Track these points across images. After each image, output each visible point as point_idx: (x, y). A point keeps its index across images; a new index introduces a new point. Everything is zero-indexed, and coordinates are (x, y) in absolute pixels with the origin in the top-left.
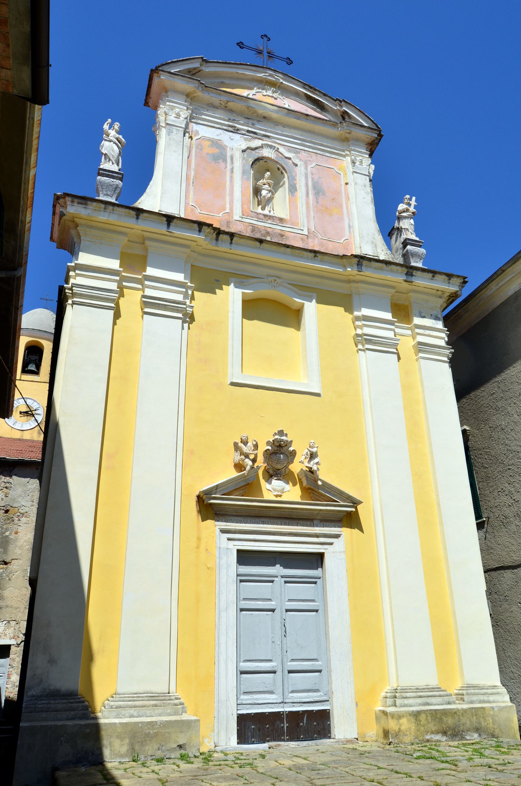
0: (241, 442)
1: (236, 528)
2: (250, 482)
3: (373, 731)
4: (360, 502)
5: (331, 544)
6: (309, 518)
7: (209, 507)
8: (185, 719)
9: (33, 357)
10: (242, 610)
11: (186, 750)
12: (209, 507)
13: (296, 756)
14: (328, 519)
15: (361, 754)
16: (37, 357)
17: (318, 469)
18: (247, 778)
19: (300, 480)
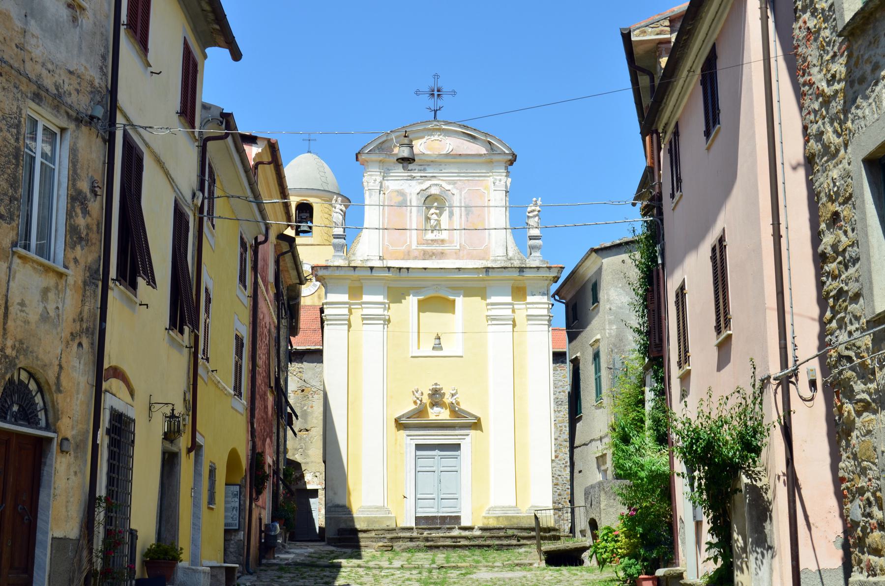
9: (304, 215)
12: (400, 425)
16: (308, 215)
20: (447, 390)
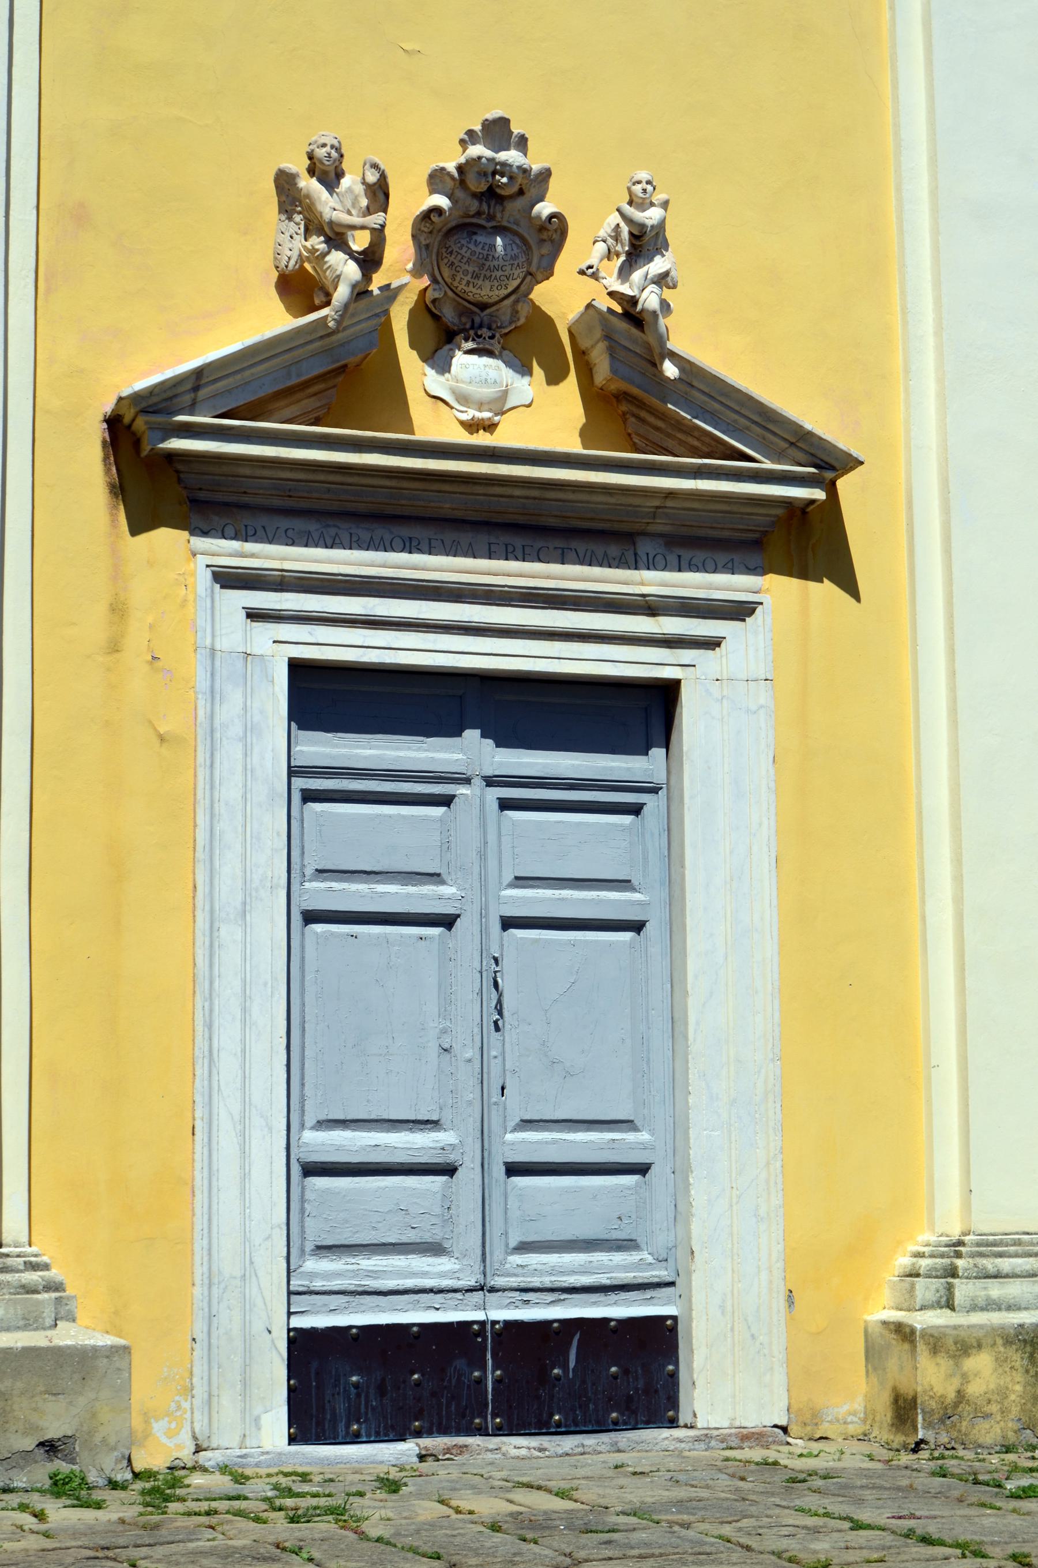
0: (311, 171)
1: (288, 565)
2: (352, 360)
3: (852, 1401)
4: (851, 463)
5: (712, 644)
6: (616, 527)
7: (159, 468)
8: (69, 1342)
10: (311, 917)
11: (73, 1461)
12: (159, 468)
13: (529, 1486)
14: (702, 533)
15: (794, 1480)
17: (665, 306)
18: (316, 1555)
19: (581, 354)
20: (586, 207)
